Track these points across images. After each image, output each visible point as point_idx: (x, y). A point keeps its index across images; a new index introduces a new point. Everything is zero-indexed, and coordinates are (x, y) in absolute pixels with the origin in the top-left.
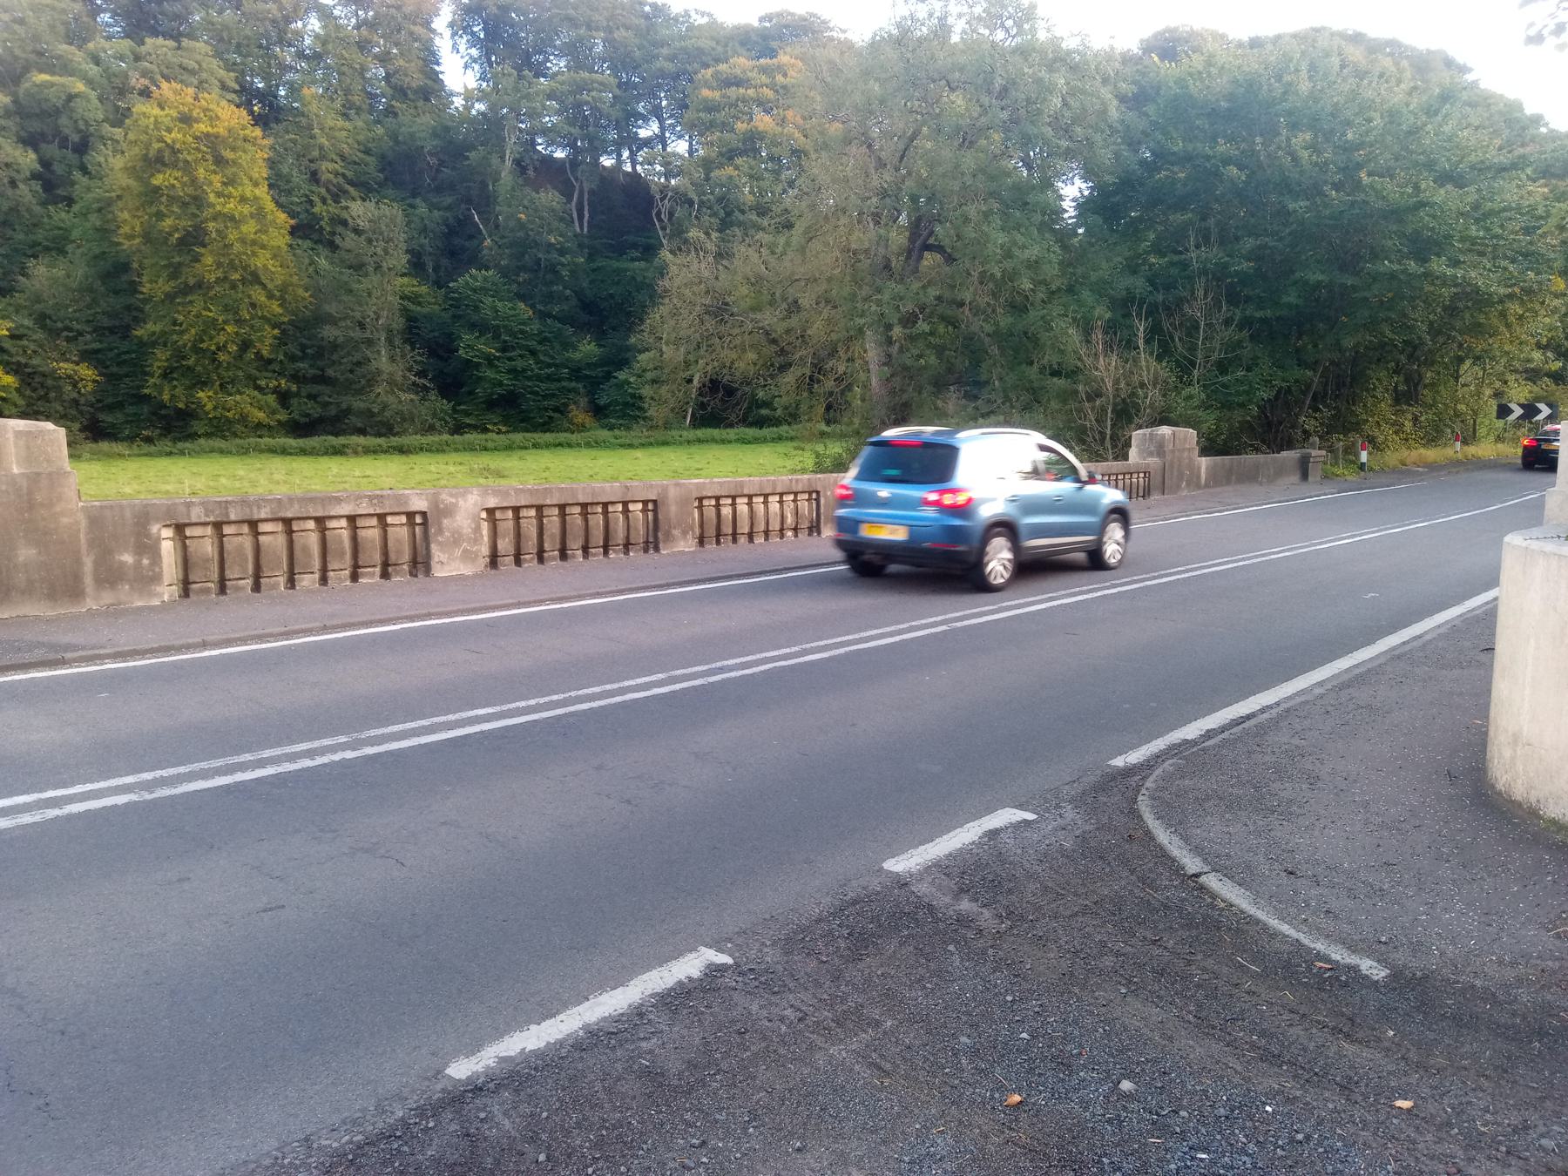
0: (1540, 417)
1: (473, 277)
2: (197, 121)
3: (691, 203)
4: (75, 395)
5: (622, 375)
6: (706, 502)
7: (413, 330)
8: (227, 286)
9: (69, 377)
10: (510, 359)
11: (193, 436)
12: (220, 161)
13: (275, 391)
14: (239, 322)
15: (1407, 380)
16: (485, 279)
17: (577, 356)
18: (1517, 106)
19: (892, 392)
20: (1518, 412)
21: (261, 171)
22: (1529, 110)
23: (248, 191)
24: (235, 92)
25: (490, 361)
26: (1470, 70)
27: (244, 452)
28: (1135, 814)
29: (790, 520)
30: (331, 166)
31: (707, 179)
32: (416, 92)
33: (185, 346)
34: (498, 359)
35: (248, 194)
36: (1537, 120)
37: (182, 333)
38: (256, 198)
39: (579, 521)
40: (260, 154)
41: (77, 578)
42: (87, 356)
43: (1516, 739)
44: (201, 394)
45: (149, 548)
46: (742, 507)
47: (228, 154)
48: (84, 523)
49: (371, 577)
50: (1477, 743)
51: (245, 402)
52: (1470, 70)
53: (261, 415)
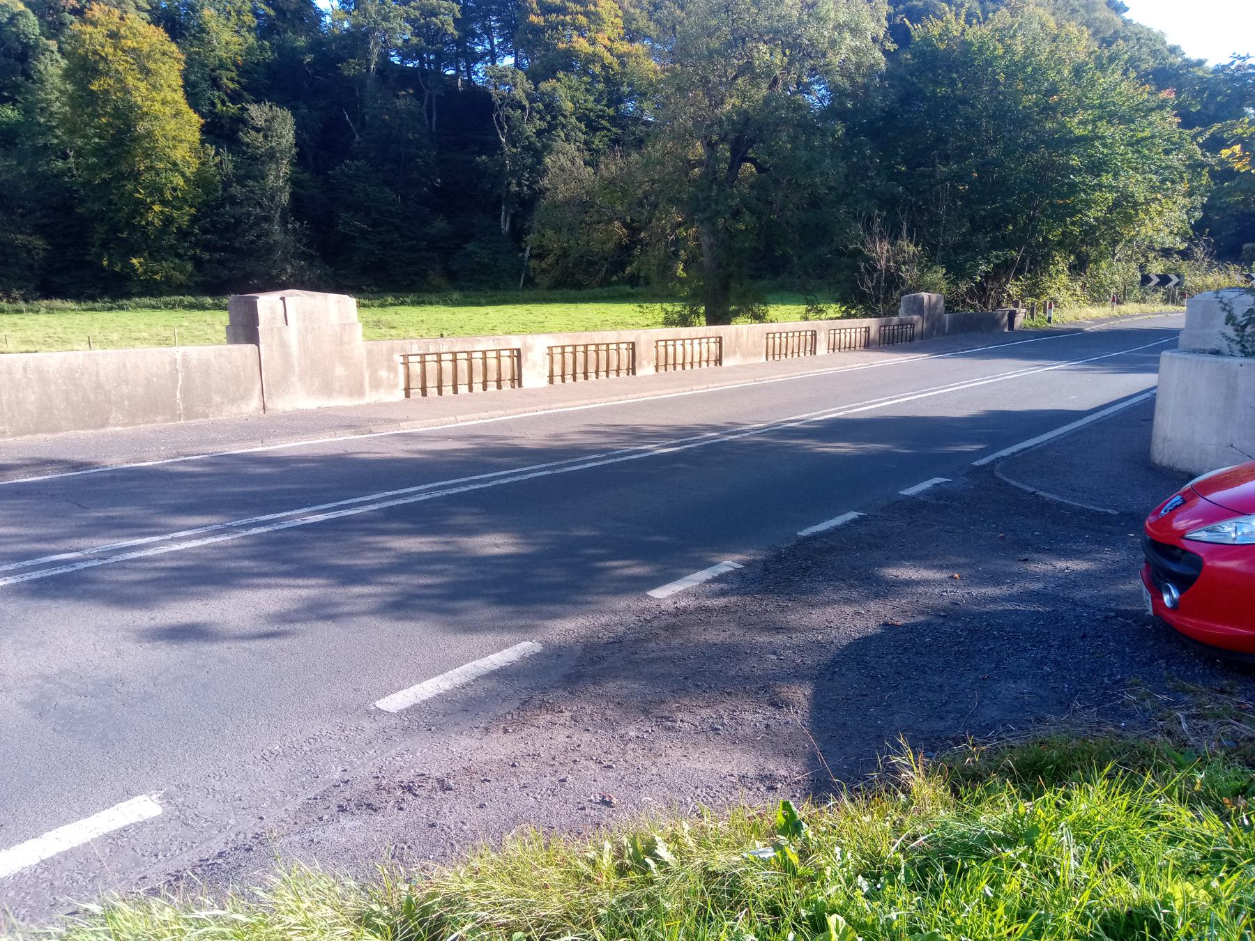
0: (1171, 284)
1: (349, 166)
2: (126, 37)
3: (523, 108)
4: (30, 261)
5: (470, 247)
6: (411, 359)
7: (298, 207)
8: (153, 173)
9: (24, 246)
10: (379, 233)
11: (129, 296)
12: (146, 72)
13: (192, 258)
14: (164, 203)
15: (1078, 257)
16: (358, 168)
17: (433, 231)
18: (1160, 38)
19: (720, 266)
20: (1156, 280)
21: (176, 81)
22: (1170, 42)
23: (170, 96)
24: (147, 11)
25: (363, 233)
26: (1126, 9)
27: (172, 307)
28: (995, 478)
29: (705, 357)
30: (230, 74)
31: (536, 89)
32: (293, 13)
33: (120, 222)
34: (370, 233)
35: (169, 98)
36: (1173, 50)
37: (117, 211)
38: (176, 102)
39: (594, 355)
40: (177, 66)
41: (362, 386)
42: (38, 230)
43: (1164, 439)
44: (134, 261)
45: (392, 368)
46: (679, 349)
47: (151, 65)
48: (365, 353)
49: (613, 375)
50: (1148, 452)
51: (164, 269)
52: (1126, 9)
53: (182, 277)
